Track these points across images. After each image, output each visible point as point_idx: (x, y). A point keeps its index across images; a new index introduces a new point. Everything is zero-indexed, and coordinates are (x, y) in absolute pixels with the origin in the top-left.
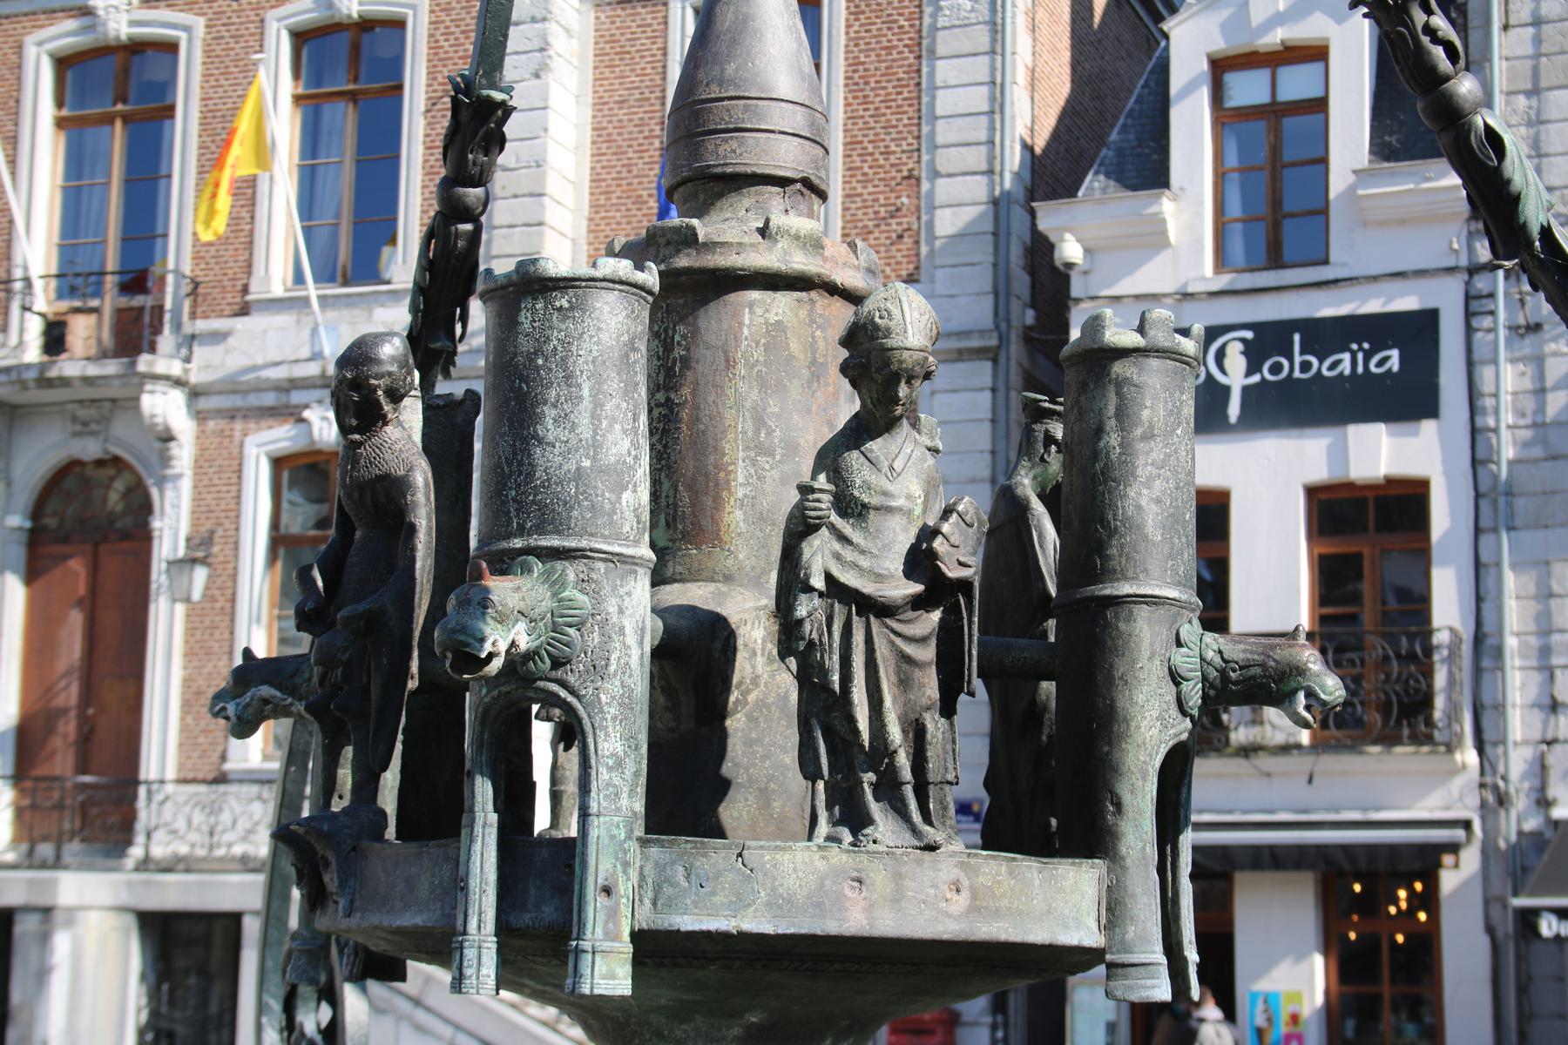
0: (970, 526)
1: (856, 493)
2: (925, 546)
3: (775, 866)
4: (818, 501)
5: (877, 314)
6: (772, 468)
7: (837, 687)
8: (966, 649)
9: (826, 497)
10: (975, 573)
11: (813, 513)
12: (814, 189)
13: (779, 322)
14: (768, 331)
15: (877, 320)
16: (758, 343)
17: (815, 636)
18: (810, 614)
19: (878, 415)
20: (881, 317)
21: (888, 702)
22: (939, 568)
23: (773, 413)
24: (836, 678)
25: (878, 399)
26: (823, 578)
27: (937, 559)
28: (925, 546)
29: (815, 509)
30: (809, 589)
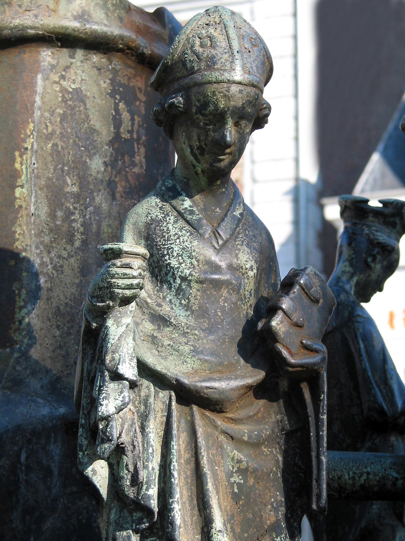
0: (317, 301)
1: (174, 263)
2: (260, 325)
3: (52, 345)
4: (128, 266)
5: (197, 42)
6: (70, 256)
7: (154, 504)
8: (314, 454)
9: (137, 263)
10: (323, 359)
11: (120, 282)
12: (130, 409)
13: (77, 91)
14: (64, 100)
15: (198, 48)
16: (52, 113)
17: (125, 439)
18: (119, 410)
19: (199, 170)
20: (202, 46)
21: (214, 502)
22: (279, 354)
23: (72, 193)
24: (153, 492)
25: (200, 148)
26: (134, 363)
27: (276, 341)
28: (260, 325)
29: (125, 276)
30: (117, 377)
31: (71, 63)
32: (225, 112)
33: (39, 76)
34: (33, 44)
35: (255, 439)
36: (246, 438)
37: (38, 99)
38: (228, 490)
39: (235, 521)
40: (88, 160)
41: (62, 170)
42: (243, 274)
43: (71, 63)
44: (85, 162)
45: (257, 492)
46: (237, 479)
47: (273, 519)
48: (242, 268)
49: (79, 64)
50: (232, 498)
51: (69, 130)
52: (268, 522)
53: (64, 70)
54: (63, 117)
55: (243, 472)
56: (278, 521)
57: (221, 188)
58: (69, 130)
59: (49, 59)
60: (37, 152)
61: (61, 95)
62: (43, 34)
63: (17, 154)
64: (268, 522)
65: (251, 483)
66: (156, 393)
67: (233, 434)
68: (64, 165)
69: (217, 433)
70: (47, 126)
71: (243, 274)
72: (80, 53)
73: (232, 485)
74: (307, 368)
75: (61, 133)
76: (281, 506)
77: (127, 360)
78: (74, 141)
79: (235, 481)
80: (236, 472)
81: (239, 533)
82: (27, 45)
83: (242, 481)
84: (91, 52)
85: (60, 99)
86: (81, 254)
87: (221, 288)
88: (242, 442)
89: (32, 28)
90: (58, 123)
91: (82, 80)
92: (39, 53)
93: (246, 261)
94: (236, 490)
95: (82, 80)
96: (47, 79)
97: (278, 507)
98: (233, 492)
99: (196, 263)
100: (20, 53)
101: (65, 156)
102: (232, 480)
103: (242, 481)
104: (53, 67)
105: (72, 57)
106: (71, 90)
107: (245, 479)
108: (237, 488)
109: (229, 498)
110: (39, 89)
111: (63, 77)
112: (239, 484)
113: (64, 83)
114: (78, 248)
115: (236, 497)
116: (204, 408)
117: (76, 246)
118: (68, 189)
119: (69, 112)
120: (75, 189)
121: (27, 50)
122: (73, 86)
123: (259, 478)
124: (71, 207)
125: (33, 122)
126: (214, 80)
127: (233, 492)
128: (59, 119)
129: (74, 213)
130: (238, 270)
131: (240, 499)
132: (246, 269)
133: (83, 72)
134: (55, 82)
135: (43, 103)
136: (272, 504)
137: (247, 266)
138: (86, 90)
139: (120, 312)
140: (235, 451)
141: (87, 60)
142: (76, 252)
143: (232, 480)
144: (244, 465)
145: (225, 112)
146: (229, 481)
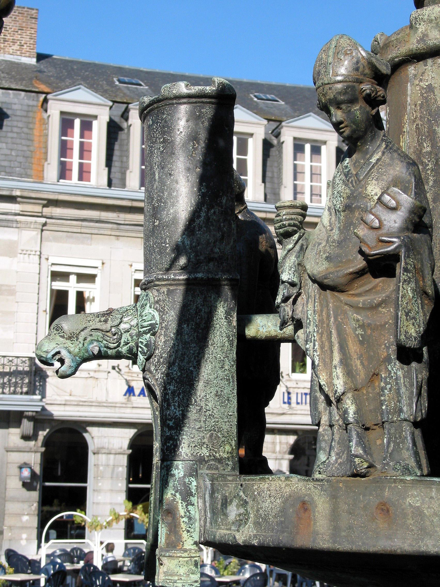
14: (422, 94)
23: (427, 152)
31: (425, 70)
32: (327, 103)
33: (409, 84)
34: (403, 66)
35: (367, 305)
36: (361, 305)
37: (409, 99)
38: (356, 340)
39: (363, 358)
40: (436, 128)
41: (422, 139)
42: (370, 200)
43: (425, 70)
44: (435, 130)
45: (374, 338)
46: (359, 331)
47: (385, 354)
48: (369, 195)
49: (430, 68)
50: (359, 344)
51: (425, 113)
52: (382, 356)
53: (422, 76)
54: (421, 106)
55: (362, 326)
56: (389, 355)
57: (364, 146)
58: (425, 113)
59: (413, 72)
60: (409, 132)
61: (420, 92)
62: (403, 59)
63: (401, 136)
64: (382, 356)
65: (369, 333)
66: (312, 285)
67: (351, 304)
68: (422, 136)
69: (343, 305)
70: (413, 114)
71: (370, 200)
72: (430, 61)
73: (357, 336)
74: (385, 255)
75: (420, 116)
76: (392, 345)
77: (287, 270)
78: (428, 118)
79: (359, 333)
80: (358, 327)
81: (367, 365)
82: (400, 68)
83: (363, 333)
84: (436, 58)
85: (419, 95)
86: (433, 190)
87: (355, 212)
88: (360, 308)
89: (397, 57)
90: (419, 111)
91: (432, 77)
92: (407, 70)
93: (372, 190)
94: (361, 339)
95: (432, 77)
96: (413, 84)
97: (390, 346)
98: (359, 340)
99: (342, 199)
100: (399, 74)
101: (422, 129)
102: (357, 332)
103: (363, 333)
104: (415, 76)
105: (426, 65)
106: (425, 87)
107: (364, 330)
108: (361, 337)
109: (358, 344)
110: (409, 92)
111: (421, 80)
112: (361, 335)
113: (421, 84)
114: (432, 186)
115: (362, 343)
116: (334, 291)
117: (430, 185)
118: (424, 151)
119: (424, 101)
120: (429, 149)
121: (402, 70)
122: (427, 84)
123: (374, 329)
124: (427, 161)
125: (407, 114)
126: (326, 82)
127: (359, 340)
128: (419, 108)
129: (428, 165)
130: (366, 197)
131: (364, 344)
132: (372, 195)
133: (432, 72)
134: (417, 85)
135: (411, 100)
136: (385, 345)
137: (372, 194)
138: (434, 83)
139: (287, 242)
140: (354, 315)
141: (434, 64)
142: (430, 189)
143: (357, 332)
144: (361, 323)
145: (327, 103)
146: (355, 334)
